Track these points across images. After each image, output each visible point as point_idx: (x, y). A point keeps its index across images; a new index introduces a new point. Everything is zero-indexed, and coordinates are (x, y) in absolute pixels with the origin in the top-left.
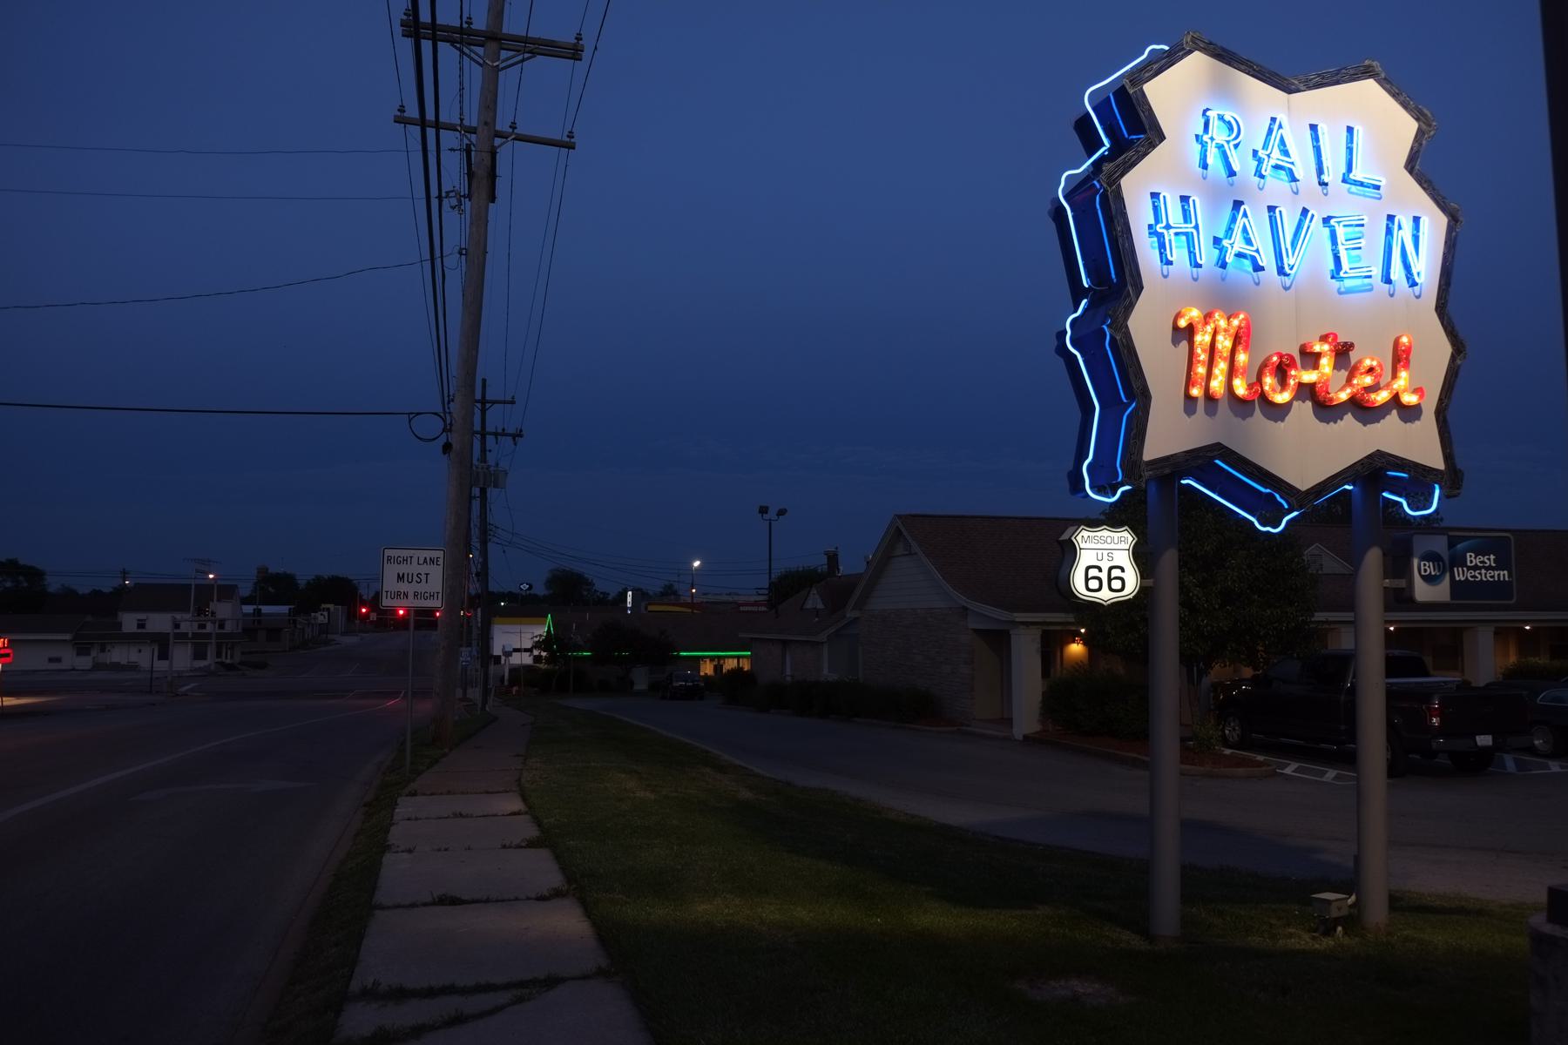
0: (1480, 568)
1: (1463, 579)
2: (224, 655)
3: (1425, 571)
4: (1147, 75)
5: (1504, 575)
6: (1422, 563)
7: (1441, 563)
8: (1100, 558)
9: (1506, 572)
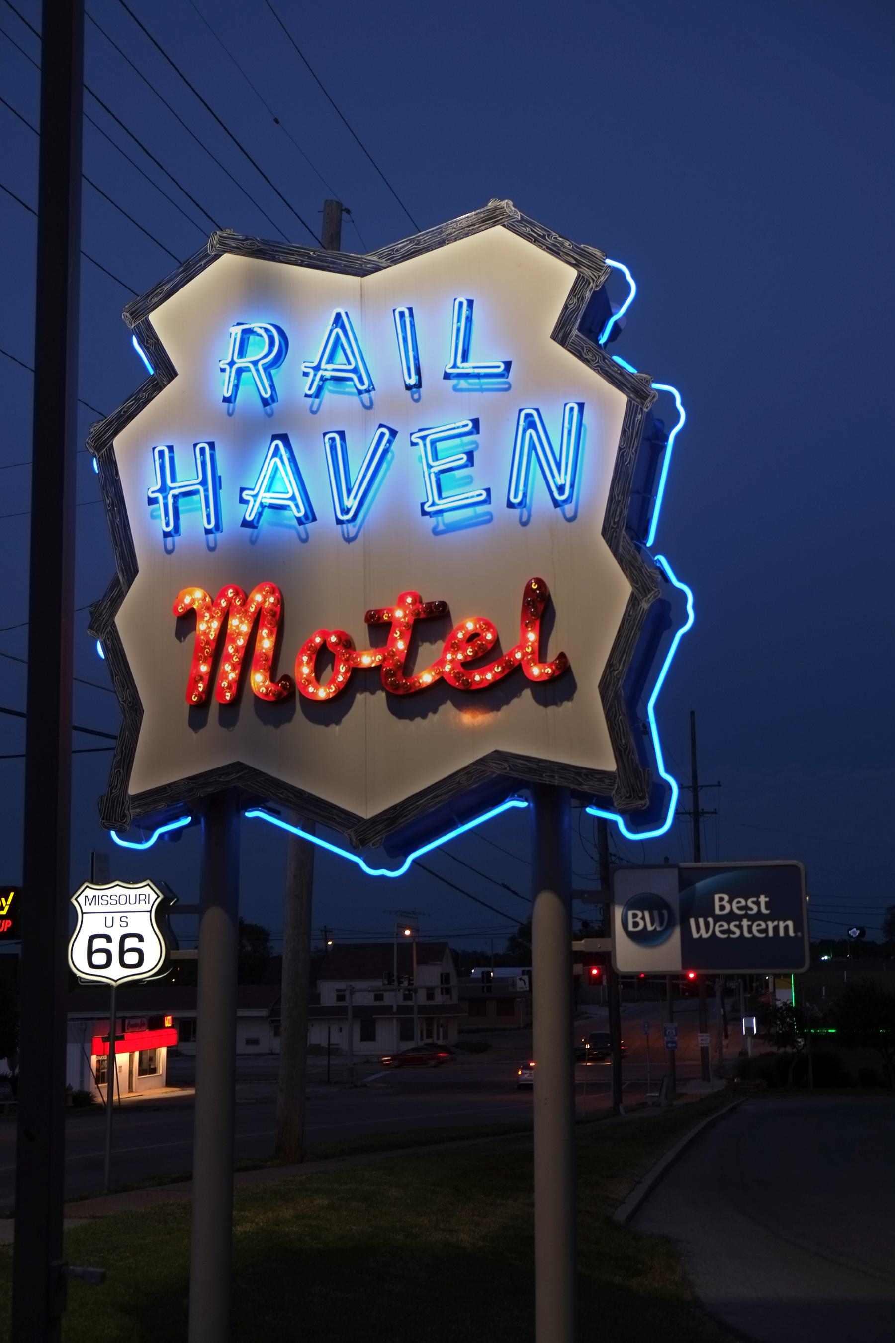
0: (740, 918)
1: (705, 935)
2: (435, 1036)
3: (636, 924)
4: (155, 300)
5: (786, 928)
6: (630, 913)
7: (665, 912)
8: (109, 923)
9: (790, 923)
